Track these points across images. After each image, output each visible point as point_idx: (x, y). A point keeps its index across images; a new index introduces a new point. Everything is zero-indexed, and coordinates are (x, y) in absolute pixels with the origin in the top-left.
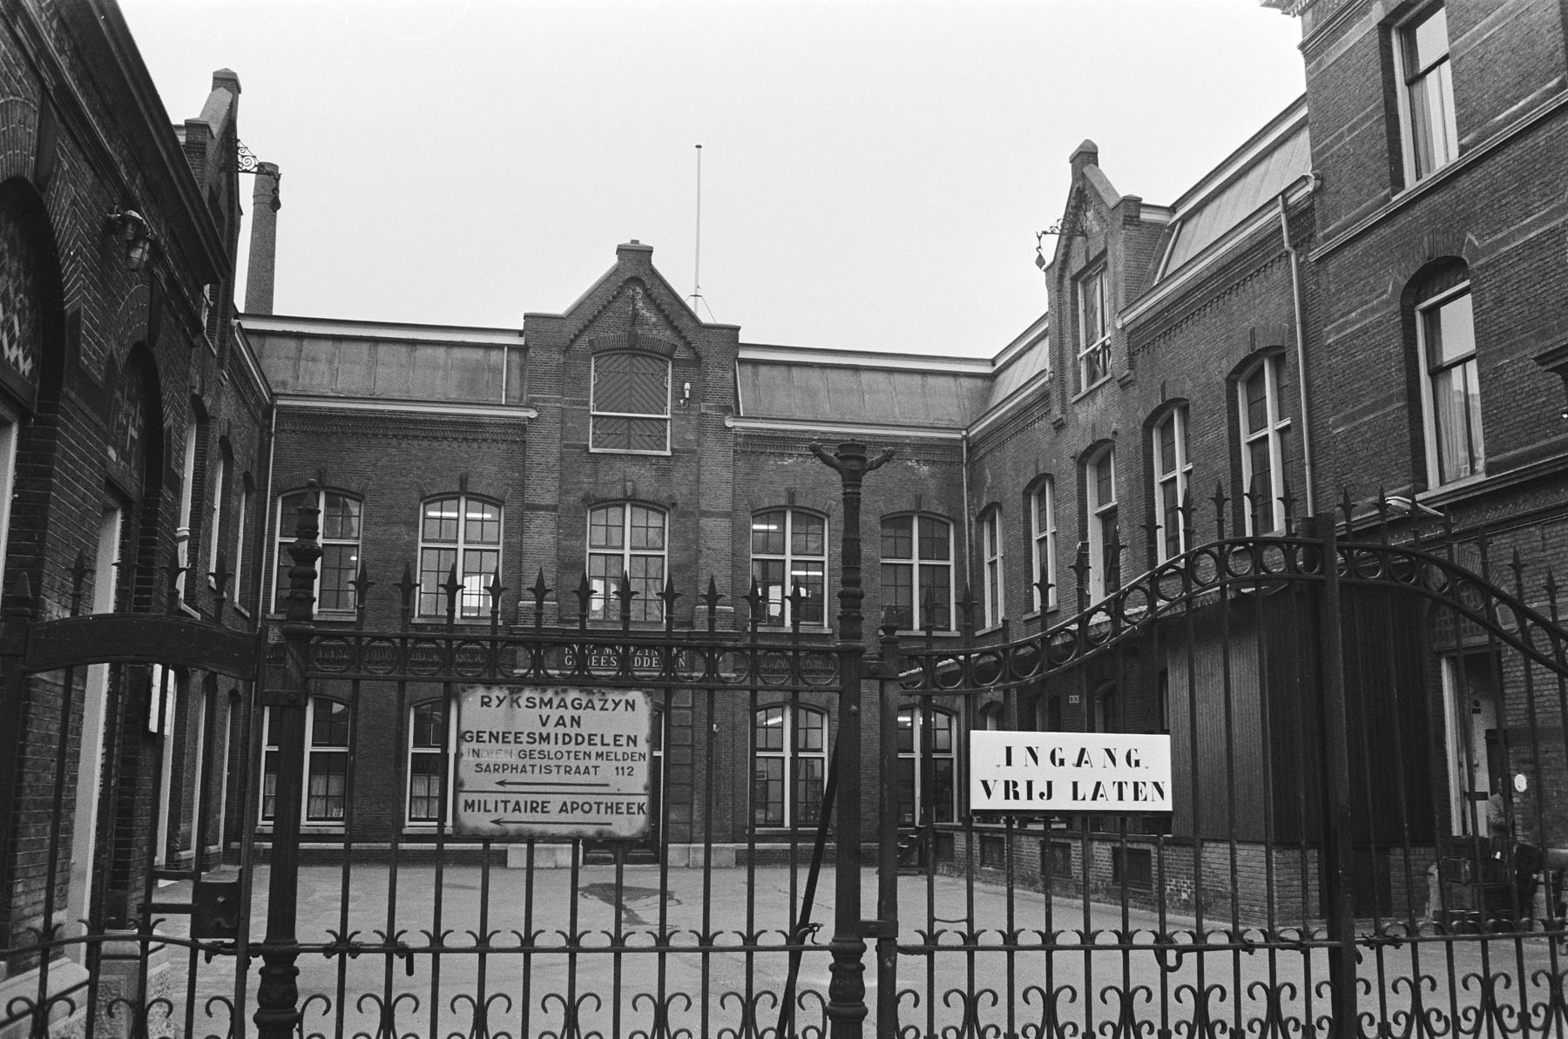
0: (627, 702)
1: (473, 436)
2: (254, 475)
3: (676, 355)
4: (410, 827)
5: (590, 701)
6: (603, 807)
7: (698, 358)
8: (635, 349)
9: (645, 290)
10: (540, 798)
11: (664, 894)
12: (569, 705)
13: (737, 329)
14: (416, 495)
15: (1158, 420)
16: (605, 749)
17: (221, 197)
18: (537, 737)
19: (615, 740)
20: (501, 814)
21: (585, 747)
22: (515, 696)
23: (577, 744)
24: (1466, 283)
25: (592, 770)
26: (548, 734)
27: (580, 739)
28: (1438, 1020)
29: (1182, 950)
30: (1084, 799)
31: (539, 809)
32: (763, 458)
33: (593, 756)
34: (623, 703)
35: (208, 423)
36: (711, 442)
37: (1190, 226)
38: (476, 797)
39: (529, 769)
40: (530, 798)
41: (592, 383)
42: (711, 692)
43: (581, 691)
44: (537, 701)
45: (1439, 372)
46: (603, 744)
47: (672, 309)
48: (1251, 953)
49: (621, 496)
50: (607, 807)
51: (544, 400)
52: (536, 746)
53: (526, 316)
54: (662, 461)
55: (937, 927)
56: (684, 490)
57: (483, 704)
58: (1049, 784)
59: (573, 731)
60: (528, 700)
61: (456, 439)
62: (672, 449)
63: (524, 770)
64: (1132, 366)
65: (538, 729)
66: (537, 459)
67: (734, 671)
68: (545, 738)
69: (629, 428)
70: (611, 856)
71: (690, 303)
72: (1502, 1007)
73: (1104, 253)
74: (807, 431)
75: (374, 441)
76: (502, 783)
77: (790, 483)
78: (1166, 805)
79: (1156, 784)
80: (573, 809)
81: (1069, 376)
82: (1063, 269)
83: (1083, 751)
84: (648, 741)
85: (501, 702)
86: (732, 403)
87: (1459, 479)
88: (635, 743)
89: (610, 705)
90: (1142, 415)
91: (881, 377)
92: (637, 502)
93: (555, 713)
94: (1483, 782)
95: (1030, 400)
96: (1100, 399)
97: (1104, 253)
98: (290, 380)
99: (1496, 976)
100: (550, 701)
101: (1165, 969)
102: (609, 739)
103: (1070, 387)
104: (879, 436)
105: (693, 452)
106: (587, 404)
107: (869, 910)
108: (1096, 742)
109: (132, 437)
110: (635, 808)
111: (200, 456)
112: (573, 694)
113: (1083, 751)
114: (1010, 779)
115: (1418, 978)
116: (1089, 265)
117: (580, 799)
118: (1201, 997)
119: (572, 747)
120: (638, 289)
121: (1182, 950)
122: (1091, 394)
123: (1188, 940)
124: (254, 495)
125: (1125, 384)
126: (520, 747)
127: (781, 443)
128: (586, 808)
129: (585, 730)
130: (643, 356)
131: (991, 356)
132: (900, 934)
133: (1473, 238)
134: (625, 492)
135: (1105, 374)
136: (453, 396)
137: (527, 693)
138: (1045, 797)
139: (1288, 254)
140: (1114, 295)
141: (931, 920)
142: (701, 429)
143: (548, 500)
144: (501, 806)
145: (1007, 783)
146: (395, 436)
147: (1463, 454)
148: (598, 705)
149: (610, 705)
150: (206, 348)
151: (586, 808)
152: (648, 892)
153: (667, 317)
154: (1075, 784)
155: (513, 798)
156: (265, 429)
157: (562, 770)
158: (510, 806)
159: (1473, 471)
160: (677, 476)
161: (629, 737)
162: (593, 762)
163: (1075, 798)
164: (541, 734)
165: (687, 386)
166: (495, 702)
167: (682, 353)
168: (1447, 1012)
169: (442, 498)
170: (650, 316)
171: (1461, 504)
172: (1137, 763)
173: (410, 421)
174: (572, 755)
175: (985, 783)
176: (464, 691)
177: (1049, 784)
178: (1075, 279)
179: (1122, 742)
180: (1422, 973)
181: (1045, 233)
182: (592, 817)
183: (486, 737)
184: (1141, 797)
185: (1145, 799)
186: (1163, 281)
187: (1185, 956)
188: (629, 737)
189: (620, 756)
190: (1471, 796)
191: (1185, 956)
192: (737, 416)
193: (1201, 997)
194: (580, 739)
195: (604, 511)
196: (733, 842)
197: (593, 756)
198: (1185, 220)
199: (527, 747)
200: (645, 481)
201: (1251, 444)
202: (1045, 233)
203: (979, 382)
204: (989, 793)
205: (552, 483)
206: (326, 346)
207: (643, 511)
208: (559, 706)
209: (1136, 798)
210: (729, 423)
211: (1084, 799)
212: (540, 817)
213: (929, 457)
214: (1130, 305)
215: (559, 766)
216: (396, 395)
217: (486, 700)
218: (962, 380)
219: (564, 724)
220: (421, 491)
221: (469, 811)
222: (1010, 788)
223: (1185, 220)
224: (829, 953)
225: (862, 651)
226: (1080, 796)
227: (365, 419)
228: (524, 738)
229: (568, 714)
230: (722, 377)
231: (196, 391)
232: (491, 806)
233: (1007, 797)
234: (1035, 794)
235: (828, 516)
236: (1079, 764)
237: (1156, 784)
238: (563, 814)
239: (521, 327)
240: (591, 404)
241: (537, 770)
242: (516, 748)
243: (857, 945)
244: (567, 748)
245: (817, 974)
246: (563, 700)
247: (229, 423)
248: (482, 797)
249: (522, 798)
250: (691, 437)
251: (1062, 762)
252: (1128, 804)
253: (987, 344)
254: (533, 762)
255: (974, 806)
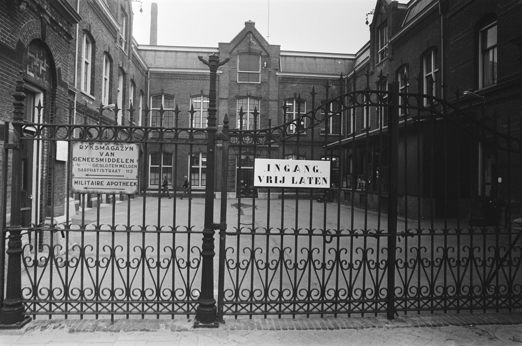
0: (130, 148)
1: (204, 79)
2: (144, 91)
3: (262, 54)
4: (150, 186)
5: (117, 147)
6: (122, 184)
7: (268, 54)
8: (250, 52)
9: (253, 35)
10: (100, 180)
11: (254, 207)
12: (110, 149)
13: (280, 46)
14: (189, 95)
15: (400, 70)
16: (123, 164)
17: (126, 8)
18: (99, 159)
19: (126, 161)
20: (87, 186)
21: (116, 163)
22: (91, 146)
23: (113, 162)
24: (496, 22)
25: (118, 171)
26: (103, 159)
27: (114, 160)
28: (427, 262)
29: (332, 236)
30: (296, 183)
31: (100, 184)
32: (287, 84)
33: (119, 166)
34: (129, 148)
35: (126, 75)
36: (272, 79)
37: (413, 10)
38: (78, 180)
39: (96, 170)
40: (97, 180)
41: (238, 63)
42: (191, 145)
43: (114, 144)
44: (99, 147)
45: (486, 51)
46: (122, 162)
47: (260, 40)
48: (357, 238)
49: (246, 95)
50: (123, 184)
51: (225, 68)
52: (99, 163)
53: (219, 44)
54: (258, 85)
55: (241, 226)
56: (265, 93)
57: (80, 148)
58: (284, 178)
59: (111, 158)
60: (96, 147)
61: (199, 79)
62: (261, 82)
63: (95, 171)
64: (393, 54)
65: (99, 157)
66: (223, 85)
67: (279, 145)
68: (102, 160)
69: (249, 76)
70: (244, 196)
71: (266, 39)
72: (450, 259)
73: (387, 19)
74: (300, 76)
75: (177, 80)
76: (87, 175)
77: (295, 91)
78: (328, 186)
79: (324, 179)
80: (111, 184)
81: (375, 58)
82: (375, 25)
83: (297, 166)
84: (137, 161)
85: (87, 147)
86: (278, 68)
87: (489, 85)
88: (133, 162)
89: (124, 149)
90: (395, 69)
91: (322, 60)
92: (251, 97)
93: (105, 152)
94: (489, 179)
95: (364, 66)
96: (384, 65)
97: (387, 19)
98: (153, 64)
99: (449, 248)
100: (104, 147)
101: (325, 242)
102: (124, 160)
103: (376, 61)
104: (321, 77)
105: (267, 82)
106: (236, 69)
107: (217, 219)
108: (302, 163)
109: (42, 70)
110: (133, 184)
111: (124, 84)
112: (111, 145)
113: (297, 166)
114: (269, 176)
115: (420, 248)
116: (382, 24)
117: (114, 181)
118: (338, 253)
119: (111, 163)
120: (251, 35)
121: (332, 236)
122: (382, 63)
123: (334, 233)
124: (144, 96)
125: (391, 60)
126: (93, 163)
127: (292, 79)
128: (116, 184)
129: (116, 157)
130: (253, 55)
131: (355, 53)
132: (227, 228)
133: (500, 6)
134: (248, 94)
135: (386, 57)
136: (199, 67)
137: (95, 144)
138: (282, 182)
139: (440, 16)
140: (389, 33)
141: (239, 224)
142: (269, 76)
143: (226, 96)
144: (87, 183)
145: (268, 177)
146: (183, 79)
147: (491, 78)
148: (120, 148)
149: (124, 149)
150: (124, 54)
151: (116, 184)
152: (249, 206)
153: (259, 43)
154: (293, 178)
155: (91, 180)
156: (146, 77)
157: (108, 171)
158: (90, 183)
159: (493, 83)
160: (263, 90)
161: (131, 160)
162: (119, 168)
163: (293, 183)
164: (100, 159)
165: (265, 63)
166: (84, 148)
167: (264, 54)
168: (430, 259)
169: (196, 96)
170: (255, 43)
171: (488, 93)
172: (317, 171)
173: (187, 74)
174: (111, 166)
175: (259, 177)
176: (74, 144)
177: (284, 178)
178: (378, 28)
179: (311, 163)
180: (421, 246)
181: (369, 14)
182: (118, 187)
183: (81, 159)
184: (318, 183)
185: (320, 184)
186: (405, 26)
187: (334, 238)
188: (131, 160)
189: (128, 166)
190: (484, 183)
191: (334, 238)
192: (280, 72)
193: (338, 253)
194: (114, 160)
195: (241, 100)
196: (278, 192)
197: (119, 166)
198: (411, 8)
199: (96, 163)
200: (253, 92)
201: (426, 77)
202: (369, 14)
203: (351, 61)
204: (261, 181)
205: (227, 92)
206: (163, 54)
207: (253, 100)
208: (107, 149)
209: (316, 183)
210: (277, 74)
211: (296, 183)
212: (100, 186)
213: (336, 83)
214: (393, 35)
215: (107, 170)
216: (183, 67)
217: (81, 147)
218: (346, 61)
219: (108, 155)
220: (190, 95)
221: (76, 184)
222: (269, 179)
223: (411, 8)
224: (202, 235)
225: (216, 130)
226: (295, 182)
227: (174, 74)
228: (95, 160)
229: (110, 152)
230: (275, 60)
231: (121, 66)
232: (83, 183)
233: (268, 182)
234: (278, 181)
235: (306, 101)
236: (295, 171)
237: (324, 179)
238: (92, 185)
239: (218, 47)
240: (238, 69)
241: (99, 170)
242: (92, 163)
243: (211, 232)
244: (109, 163)
245: (197, 240)
246: (108, 147)
247: (134, 76)
248: (81, 180)
249: (94, 180)
250: (266, 78)
251: (289, 170)
252: (313, 185)
253: (354, 50)
254: (98, 168)
255: (255, 185)
